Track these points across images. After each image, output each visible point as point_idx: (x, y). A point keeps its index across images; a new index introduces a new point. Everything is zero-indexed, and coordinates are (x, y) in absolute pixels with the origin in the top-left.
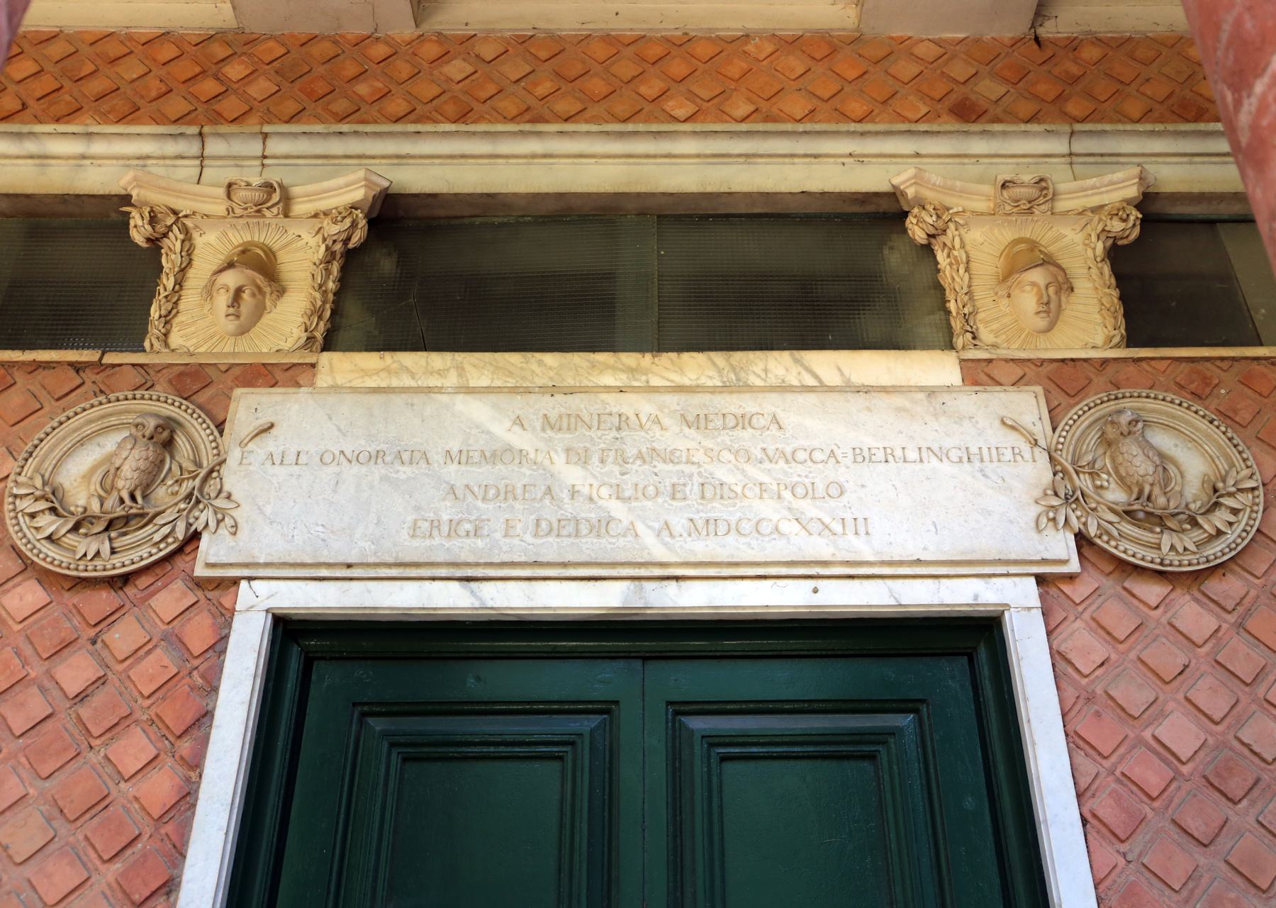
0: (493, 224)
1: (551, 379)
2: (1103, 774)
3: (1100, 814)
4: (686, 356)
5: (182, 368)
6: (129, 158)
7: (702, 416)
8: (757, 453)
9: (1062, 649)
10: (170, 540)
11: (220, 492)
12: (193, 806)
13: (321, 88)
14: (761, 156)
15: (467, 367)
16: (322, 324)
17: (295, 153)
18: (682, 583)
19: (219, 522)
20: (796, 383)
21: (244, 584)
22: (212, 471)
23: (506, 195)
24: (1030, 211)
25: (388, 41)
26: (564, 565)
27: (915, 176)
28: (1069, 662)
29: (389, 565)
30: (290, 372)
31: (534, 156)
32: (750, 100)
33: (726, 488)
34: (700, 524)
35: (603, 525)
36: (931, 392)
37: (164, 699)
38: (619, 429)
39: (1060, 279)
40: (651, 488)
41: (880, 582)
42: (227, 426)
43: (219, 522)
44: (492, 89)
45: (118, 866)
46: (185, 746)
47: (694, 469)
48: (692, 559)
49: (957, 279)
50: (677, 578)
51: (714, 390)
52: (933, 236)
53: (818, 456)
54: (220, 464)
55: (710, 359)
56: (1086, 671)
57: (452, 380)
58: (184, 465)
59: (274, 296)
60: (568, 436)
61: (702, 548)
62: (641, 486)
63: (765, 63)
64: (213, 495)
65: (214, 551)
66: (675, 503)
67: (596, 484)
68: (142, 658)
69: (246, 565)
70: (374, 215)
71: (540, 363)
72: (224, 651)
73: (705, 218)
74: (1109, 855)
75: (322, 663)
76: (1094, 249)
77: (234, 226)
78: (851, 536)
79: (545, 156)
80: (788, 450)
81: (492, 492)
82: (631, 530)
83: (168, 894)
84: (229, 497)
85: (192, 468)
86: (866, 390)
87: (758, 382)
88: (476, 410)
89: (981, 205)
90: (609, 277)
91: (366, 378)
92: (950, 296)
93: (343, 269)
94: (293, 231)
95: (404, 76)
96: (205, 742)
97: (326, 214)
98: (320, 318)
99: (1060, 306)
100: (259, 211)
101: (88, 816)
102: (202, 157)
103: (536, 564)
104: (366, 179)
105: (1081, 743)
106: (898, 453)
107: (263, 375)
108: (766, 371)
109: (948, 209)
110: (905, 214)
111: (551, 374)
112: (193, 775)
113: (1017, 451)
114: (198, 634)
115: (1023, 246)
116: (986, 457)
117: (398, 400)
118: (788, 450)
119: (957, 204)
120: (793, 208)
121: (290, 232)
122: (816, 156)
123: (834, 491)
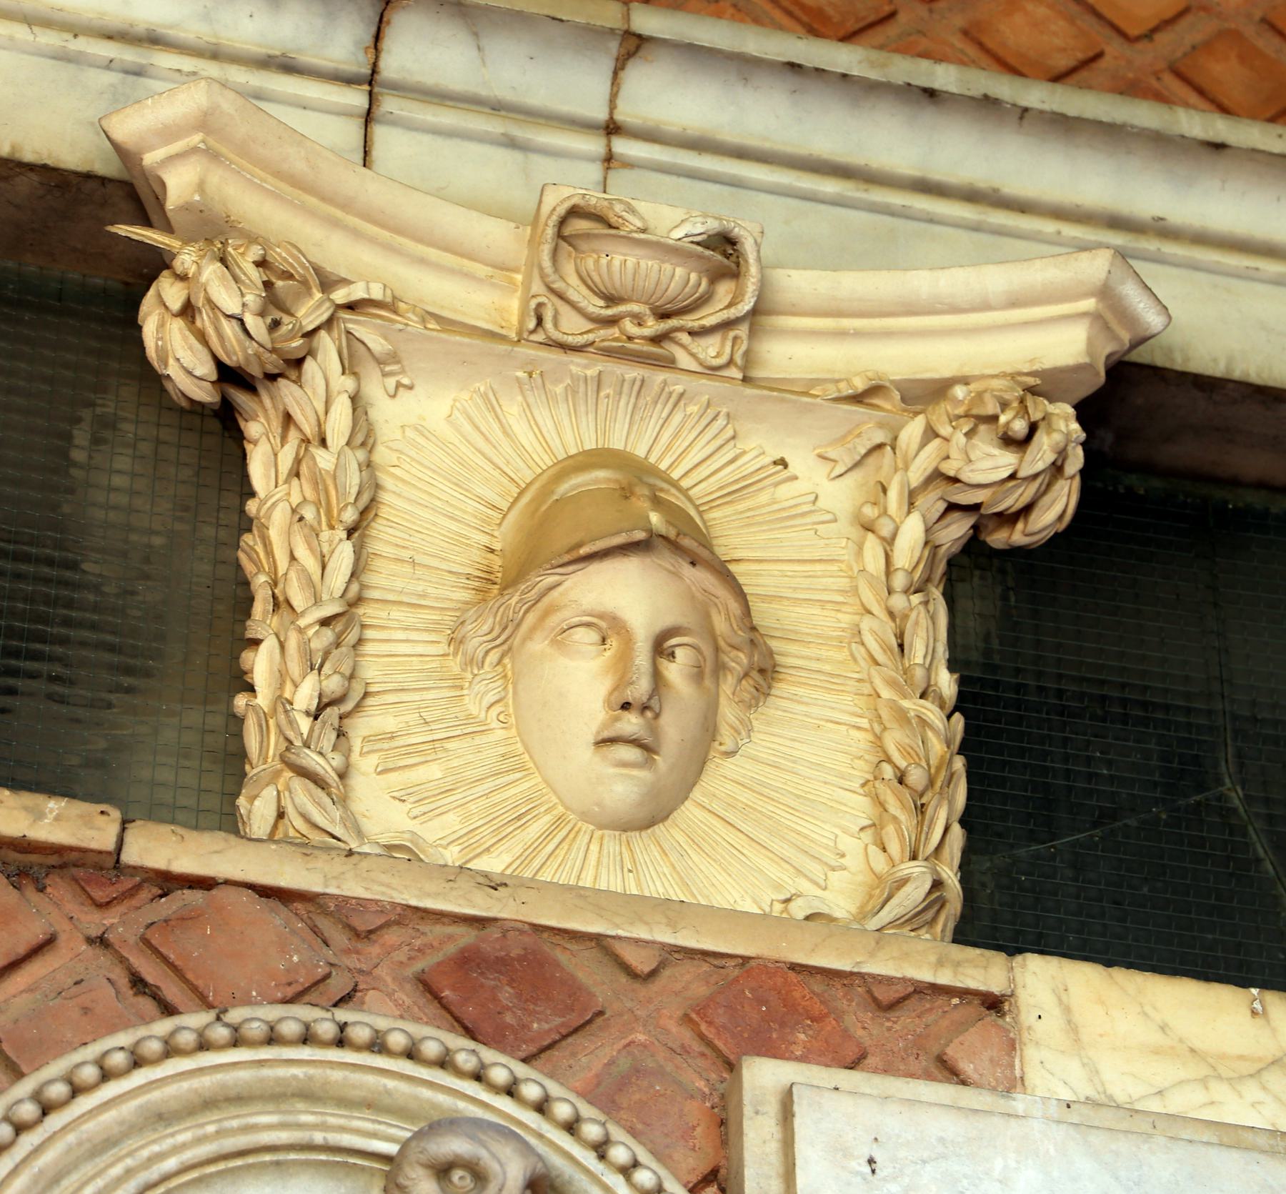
5: (466, 936)
6: (76, 29)
24: (655, 353)
39: (720, 624)
76: (889, 542)
91: (1220, 1091)
94: (760, 444)
99: (709, 730)
102: (371, 80)
104: (1105, 293)
109: (328, 283)
115: (600, 477)
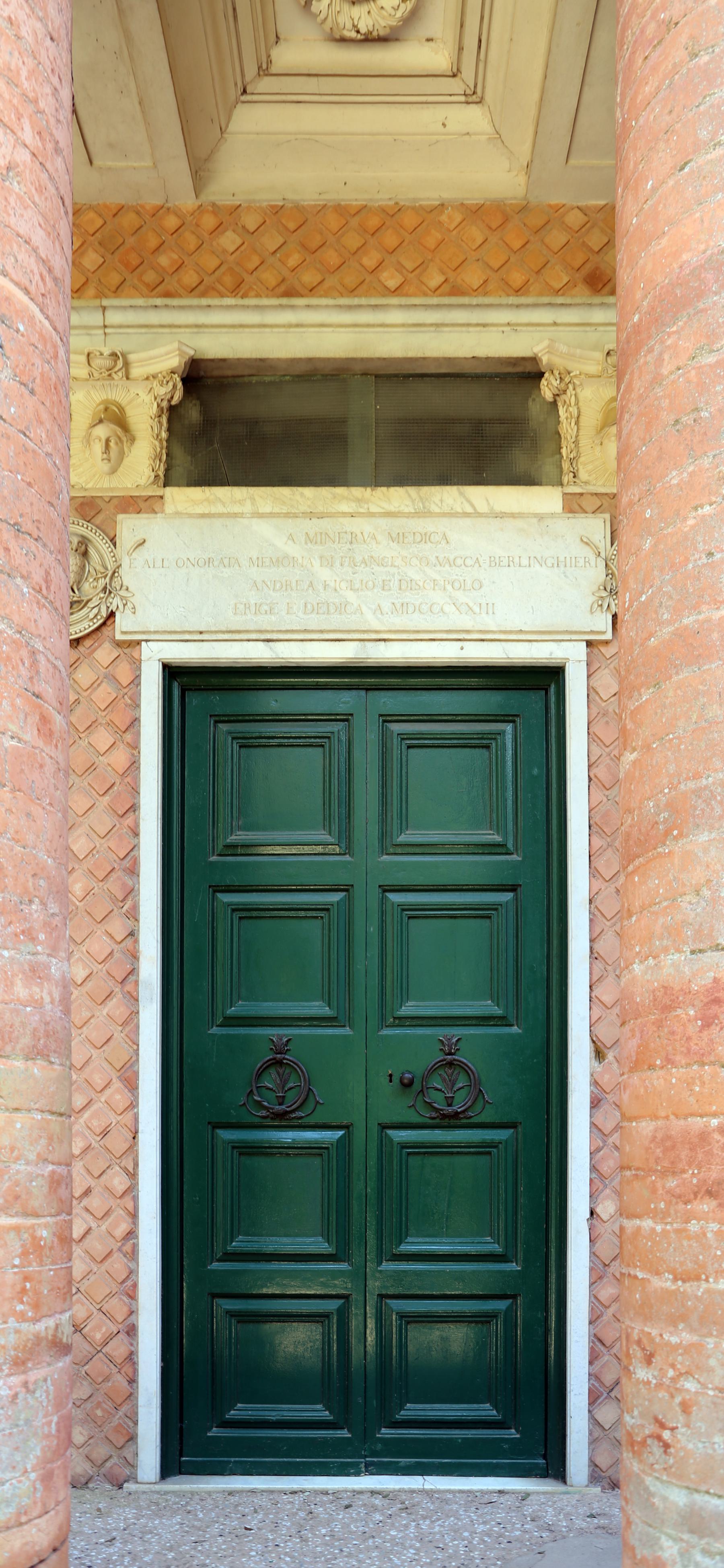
0: (264, 383)
1: (309, 506)
2: (604, 754)
3: (598, 775)
4: (393, 490)
5: (82, 500)
7: (401, 534)
8: (433, 559)
9: (594, 685)
10: (99, 617)
11: (122, 586)
12: (139, 768)
13: (134, 260)
14: (447, 325)
15: (257, 498)
16: (162, 465)
17: (125, 323)
18: (387, 643)
19: (124, 605)
20: (459, 510)
21: (143, 643)
22: (114, 572)
23: (272, 360)
25: (177, 212)
26: (321, 632)
27: (549, 346)
28: (597, 693)
29: (223, 632)
30: (148, 503)
31: (290, 326)
32: (443, 273)
33: (413, 583)
34: (398, 606)
35: (343, 607)
36: (541, 517)
37: (112, 711)
38: (351, 543)
40: (370, 583)
41: (498, 643)
42: (118, 540)
43: (124, 605)
44: (256, 261)
45: (107, 798)
46: (128, 737)
47: (395, 570)
48: (393, 629)
49: (570, 431)
50: (385, 640)
51: (408, 515)
52: (558, 395)
53: (469, 562)
54: (118, 567)
55: (407, 492)
56: (605, 698)
57: (248, 508)
58: (97, 568)
59: (129, 444)
60: (321, 548)
61: (399, 621)
62: (364, 582)
63: (454, 232)
64: (118, 588)
65: (124, 624)
66: (384, 593)
67: (338, 580)
68: (95, 689)
69: (144, 633)
70: (185, 376)
71: (302, 495)
72: (139, 684)
73: (407, 376)
74: (598, 796)
75: (191, 693)
77: (94, 387)
78: (484, 615)
79: (298, 326)
80: (452, 558)
81: (278, 586)
82: (359, 610)
83: (134, 811)
84: (127, 589)
85: (103, 570)
86: (502, 515)
87: (437, 510)
88: (264, 529)
89: (593, 369)
90: (343, 421)
92: (564, 443)
93: (169, 421)
94: (133, 391)
95: (192, 247)
96: (138, 734)
97: (154, 377)
98: (160, 460)
100: (110, 375)
101: (87, 773)
103: (306, 631)
104: (179, 349)
105: (596, 739)
106: (517, 560)
107: (131, 504)
108: (441, 501)
110: (541, 375)
111: (309, 503)
112: (136, 753)
113: (587, 560)
114: (124, 674)
116: (568, 564)
117: (218, 522)
118: (452, 558)
119: (576, 368)
120: (468, 369)
121: (132, 391)
122: (484, 325)
123: (476, 586)
